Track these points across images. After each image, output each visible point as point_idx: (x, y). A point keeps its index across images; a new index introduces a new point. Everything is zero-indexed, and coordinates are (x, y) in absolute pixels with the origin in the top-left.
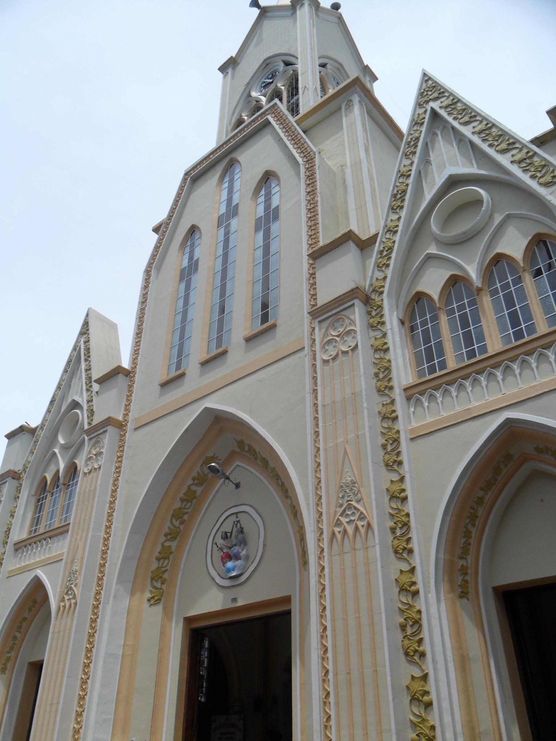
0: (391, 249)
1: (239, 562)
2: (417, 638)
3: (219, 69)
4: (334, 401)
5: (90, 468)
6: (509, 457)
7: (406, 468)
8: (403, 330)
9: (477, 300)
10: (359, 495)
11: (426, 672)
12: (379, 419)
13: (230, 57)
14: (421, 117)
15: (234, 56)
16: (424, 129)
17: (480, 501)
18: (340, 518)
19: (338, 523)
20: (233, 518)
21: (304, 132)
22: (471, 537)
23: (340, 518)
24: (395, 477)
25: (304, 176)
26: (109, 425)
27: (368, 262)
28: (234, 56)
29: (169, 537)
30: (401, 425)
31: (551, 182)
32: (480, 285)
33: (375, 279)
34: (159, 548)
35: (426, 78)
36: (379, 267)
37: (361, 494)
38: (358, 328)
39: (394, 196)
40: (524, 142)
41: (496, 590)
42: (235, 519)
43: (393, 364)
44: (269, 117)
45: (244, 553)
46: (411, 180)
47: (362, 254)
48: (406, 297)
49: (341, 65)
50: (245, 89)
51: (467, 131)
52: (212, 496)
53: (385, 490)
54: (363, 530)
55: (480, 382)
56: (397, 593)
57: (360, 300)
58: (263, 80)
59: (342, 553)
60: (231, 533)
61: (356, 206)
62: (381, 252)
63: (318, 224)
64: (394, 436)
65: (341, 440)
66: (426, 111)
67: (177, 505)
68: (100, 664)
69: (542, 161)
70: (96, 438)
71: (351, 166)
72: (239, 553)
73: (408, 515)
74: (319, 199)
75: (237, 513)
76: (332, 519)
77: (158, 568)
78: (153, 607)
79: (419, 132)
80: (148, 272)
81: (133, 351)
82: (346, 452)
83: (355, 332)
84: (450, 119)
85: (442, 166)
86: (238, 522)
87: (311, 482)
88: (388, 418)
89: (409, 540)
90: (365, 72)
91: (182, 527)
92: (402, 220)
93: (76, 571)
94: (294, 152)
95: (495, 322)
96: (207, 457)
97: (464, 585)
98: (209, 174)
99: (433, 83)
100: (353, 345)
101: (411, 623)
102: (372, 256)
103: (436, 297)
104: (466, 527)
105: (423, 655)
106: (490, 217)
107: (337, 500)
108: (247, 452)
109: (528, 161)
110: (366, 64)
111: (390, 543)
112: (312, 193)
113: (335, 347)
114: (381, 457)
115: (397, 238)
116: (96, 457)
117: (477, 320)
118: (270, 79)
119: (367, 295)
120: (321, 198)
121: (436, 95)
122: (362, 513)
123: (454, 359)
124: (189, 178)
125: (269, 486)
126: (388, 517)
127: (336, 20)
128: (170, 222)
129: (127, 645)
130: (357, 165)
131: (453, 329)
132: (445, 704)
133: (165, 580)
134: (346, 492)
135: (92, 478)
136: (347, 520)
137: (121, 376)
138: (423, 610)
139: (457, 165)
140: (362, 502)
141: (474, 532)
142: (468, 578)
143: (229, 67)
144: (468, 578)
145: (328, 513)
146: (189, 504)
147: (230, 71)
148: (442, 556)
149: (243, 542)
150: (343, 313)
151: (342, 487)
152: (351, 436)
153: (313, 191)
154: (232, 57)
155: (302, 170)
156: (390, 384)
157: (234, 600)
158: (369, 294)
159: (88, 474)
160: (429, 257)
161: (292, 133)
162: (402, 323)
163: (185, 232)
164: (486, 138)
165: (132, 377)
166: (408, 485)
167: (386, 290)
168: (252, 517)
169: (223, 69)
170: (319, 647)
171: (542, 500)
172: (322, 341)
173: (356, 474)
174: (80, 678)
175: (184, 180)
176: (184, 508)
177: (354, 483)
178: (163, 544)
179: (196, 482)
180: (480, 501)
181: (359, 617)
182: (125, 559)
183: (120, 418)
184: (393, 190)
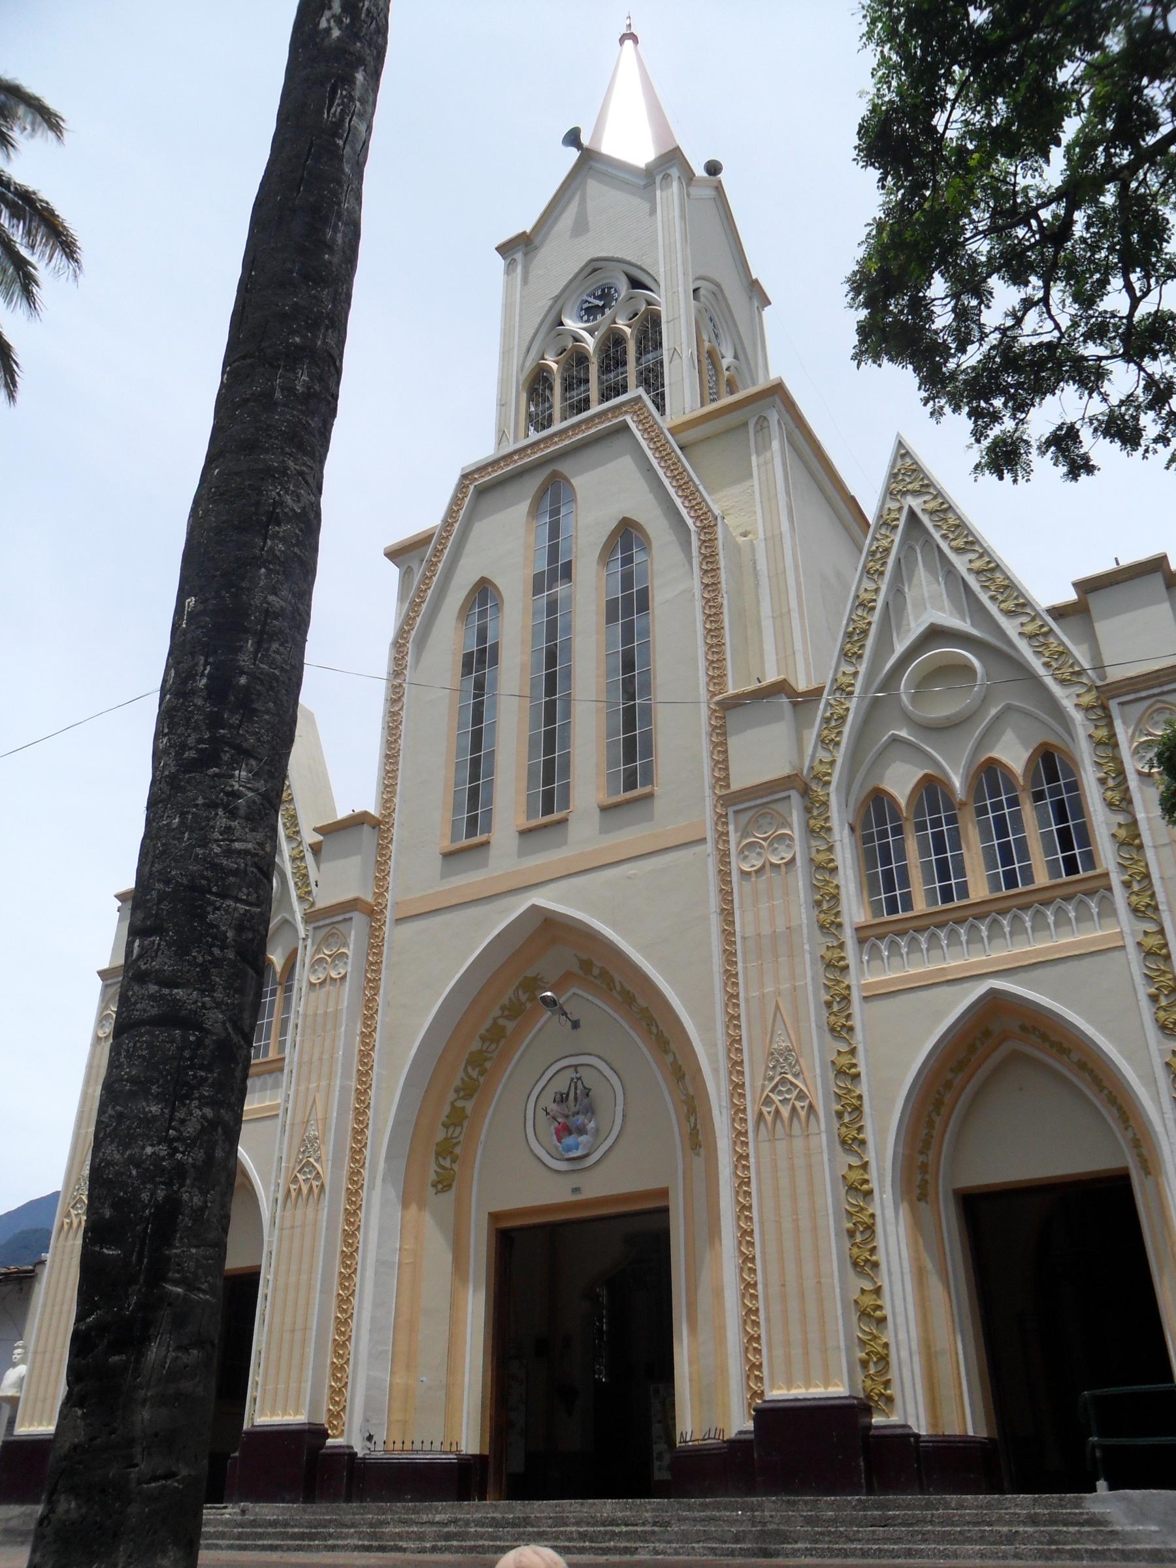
0: (842, 719)
1: (583, 1139)
2: (870, 1246)
3: (497, 249)
4: (759, 935)
5: (322, 977)
6: (987, 1034)
7: (859, 1037)
8: (853, 839)
9: (959, 817)
10: (797, 1067)
11: (879, 1284)
12: (821, 968)
13: (521, 231)
14: (893, 516)
15: (528, 231)
16: (897, 537)
17: (948, 1085)
18: (770, 1094)
19: (768, 1101)
20: (570, 1073)
21: (681, 448)
22: (933, 1128)
23: (770, 1094)
24: (844, 1048)
25: (697, 554)
26: (356, 910)
27: (806, 732)
28: (528, 231)
29: (462, 1094)
30: (852, 979)
31: (1069, 680)
32: (964, 799)
33: (817, 761)
34: (447, 1109)
35: (903, 451)
36: (824, 742)
37: (800, 1065)
38: (796, 836)
39: (849, 635)
40: (1038, 608)
41: (956, 1192)
42: (574, 1075)
43: (843, 891)
44: (628, 418)
45: (592, 1125)
46: (875, 617)
47: (794, 712)
48: (858, 793)
49: (718, 285)
50: (551, 308)
51: (960, 563)
52: (530, 1036)
53: (830, 1064)
54: (803, 1114)
55: (958, 935)
56: (844, 1192)
57: (798, 790)
58: (585, 298)
59: (773, 1139)
60: (568, 1095)
61: (773, 611)
62: (827, 720)
63: (723, 644)
64: (843, 992)
65: (769, 989)
66: (900, 509)
67: (476, 1045)
68: (370, 1273)
69: (1059, 645)
70: (329, 928)
71: (765, 539)
72: (584, 1125)
73: (860, 1097)
74: (725, 603)
75: (576, 1067)
76: (758, 1095)
77: (446, 1139)
78: (441, 1195)
79: (889, 540)
80: (399, 646)
81: (382, 788)
82: (777, 1007)
83: (791, 838)
84: (937, 536)
85: (921, 605)
86: (580, 1078)
87: (721, 1041)
88: (834, 966)
89: (860, 1129)
90: (751, 291)
91: (482, 1080)
92: (860, 677)
93: (317, 1138)
94: (678, 502)
95: (980, 852)
96: (525, 977)
97: (924, 1184)
98: (511, 490)
99: (913, 464)
100: (788, 857)
101: (861, 1229)
102: (812, 725)
103: (903, 802)
104: (929, 1116)
105: (875, 1265)
106: (983, 701)
107: (766, 1071)
108: (595, 977)
109: (1042, 639)
110: (754, 277)
111: (836, 1131)
112: (712, 588)
113: (759, 854)
114: (825, 1017)
115: (853, 704)
116: (333, 961)
117: (956, 846)
118: (599, 298)
119: (806, 784)
120: (728, 600)
121: (916, 486)
122: (801, 1090)
123: (923, 893)
124: (472, 488)
125: (633, 1034)
126: (833, 1097)
127: (712, 193)
128: (439, 561)
129: (405, 1250)
130: (774, 540)
131: (924, 852)
132: (901, 1320)
133: (457, 1157)
134: (778, 1061)
135: (328, 993)
136: (781, 1098)
137: (366, 828)
138: (878, 1213)
139: (942, 609)
140: (801, 1076)
141: (938, 1121)
142: (928, 1177)
143: (519, 250)
144: (928, 1177)
145: (753, 1086)
146: (493, 1046)
147: (519, 256)
148: (901, 1150)
149: (590, 1110)
150: (774, 806)
151: (772, 1054)
152: (785, 986)
153: (713, 584)
154: (524, 233)
155: (695, 543)
156: (838, 920)
157: (576, 1190)
158: (808, 781)
159: (318, 986)
160: (895, 740)
161: (673, 464)
162: (852, 829)
163: (470, 588)
164: (987, 584)
165: (384, 831)
166: (861, 1059)
167: (835, 779)
168: (600, 1071)
169: (505, 249)
170: (737, 1254)
171: (1021, 1089)
172: (740, 842)
173: (793, 1037)
174: (335, 1294)
175: (462, 487)
176: (486, 1051)
177: (790, 1050)
178: (452, 1104)
179: (506, 1013)
180: (948, 1085)
181: (797, 1220)
182: (397, 1124)
183: (370, 899)
184: (847, 625)
